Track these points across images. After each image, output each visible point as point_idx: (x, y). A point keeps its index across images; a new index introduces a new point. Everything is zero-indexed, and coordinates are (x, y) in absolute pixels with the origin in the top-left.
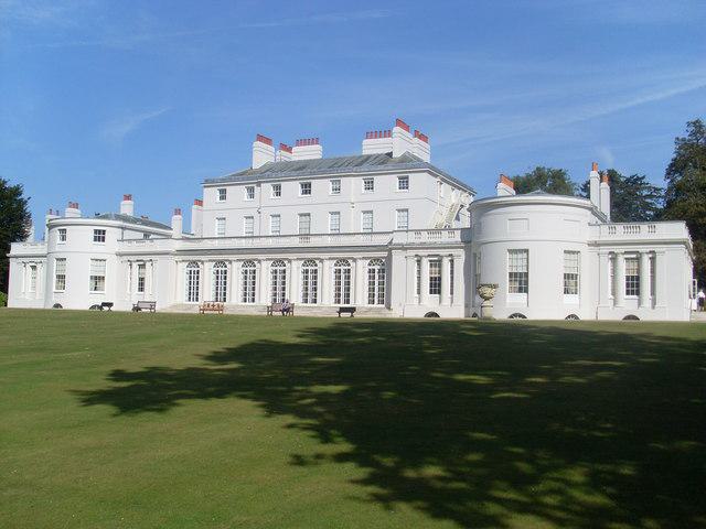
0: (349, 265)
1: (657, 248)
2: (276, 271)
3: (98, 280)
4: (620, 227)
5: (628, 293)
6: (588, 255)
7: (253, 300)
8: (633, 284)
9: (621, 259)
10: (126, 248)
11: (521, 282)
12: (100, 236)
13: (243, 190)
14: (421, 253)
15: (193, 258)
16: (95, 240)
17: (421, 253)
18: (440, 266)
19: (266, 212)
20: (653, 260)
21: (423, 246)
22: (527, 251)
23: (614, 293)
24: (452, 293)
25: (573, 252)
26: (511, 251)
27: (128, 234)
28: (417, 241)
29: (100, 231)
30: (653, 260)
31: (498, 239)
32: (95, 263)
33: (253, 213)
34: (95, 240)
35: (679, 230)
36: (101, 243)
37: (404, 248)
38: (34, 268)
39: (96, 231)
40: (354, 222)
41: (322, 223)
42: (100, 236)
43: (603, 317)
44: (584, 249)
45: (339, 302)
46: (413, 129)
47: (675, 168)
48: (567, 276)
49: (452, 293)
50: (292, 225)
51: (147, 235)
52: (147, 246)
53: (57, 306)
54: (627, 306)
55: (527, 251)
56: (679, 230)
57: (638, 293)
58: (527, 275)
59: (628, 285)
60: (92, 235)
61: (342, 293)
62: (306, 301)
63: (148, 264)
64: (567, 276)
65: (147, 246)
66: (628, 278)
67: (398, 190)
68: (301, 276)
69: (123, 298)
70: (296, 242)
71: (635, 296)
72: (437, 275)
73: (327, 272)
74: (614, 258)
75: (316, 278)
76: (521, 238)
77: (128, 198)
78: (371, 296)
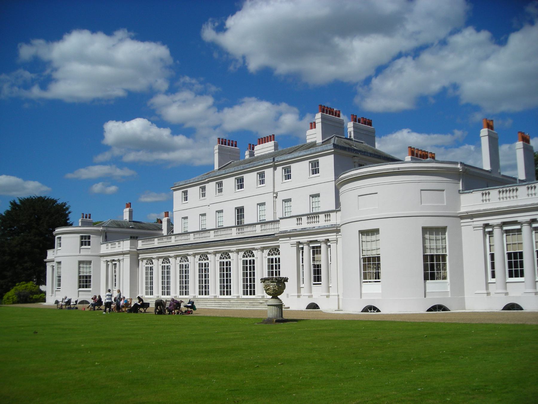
36: (87, 247)
39: (82, 237)
70: (234, 234)
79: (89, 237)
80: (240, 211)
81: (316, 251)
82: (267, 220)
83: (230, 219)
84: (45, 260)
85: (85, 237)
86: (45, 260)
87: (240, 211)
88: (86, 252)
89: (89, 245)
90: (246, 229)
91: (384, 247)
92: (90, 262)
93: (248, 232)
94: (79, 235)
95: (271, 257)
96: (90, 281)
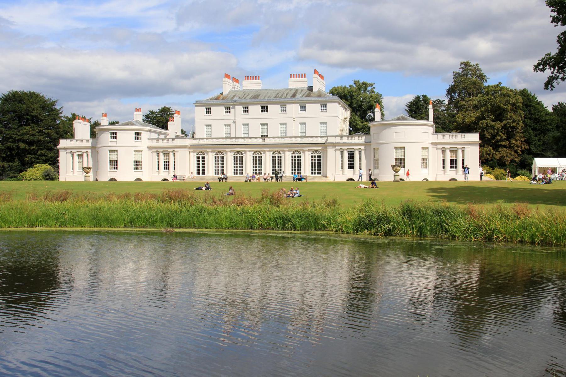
1: (175, 150)
3: (137, 164)
4: (440, 135)
5: (451, 167)
6: (432, 149)
7: (204, 174)
9: (75, 155)
10: (154, 143)
11: (115, 164)
12: (137, 136)
13: (278, 107)
14: (343, 148)
17: (343, 148)
18: (169, 156)
19: (239, 123)
20: (463, 151)
21: (345, 144)
22: (404, 148)
23: (342, 168)
24: (174, 169)
25: (139, 151)
26: (396, 148)
28: (341, 141)
29: (138, 133)
30: (463, 151)
32: (136, 153)
33: (231, 122)
35: (474, 137)
37: (334, 145)
39: (136, 134)
40: (294, 130)
41: (275, 131)
43: (439, 179)
44: (430, 146)
45: (218, 174)
46: (231, 78)
47: (451, 91)
48: (423, 159)
49: (174, 169)
50: (256, 131)
53: (112, 179)
54: (164, 174)
55: (404, 148)
56: (474, 137)
57: (456, 167)
58: (404, 159)
59: (349, 164)
62: (199, 174)
64: (423, 159)
66: (451, 160)
67: (300, 112)
68: (196, 162)
69: (151, 173)
71: (454, 169)
72: (403, 157)
73: (210, 159)
74: (444, 152)
75: (204, 161)
76: (397, 141)
78: (217, 171)
92: (374, 149)
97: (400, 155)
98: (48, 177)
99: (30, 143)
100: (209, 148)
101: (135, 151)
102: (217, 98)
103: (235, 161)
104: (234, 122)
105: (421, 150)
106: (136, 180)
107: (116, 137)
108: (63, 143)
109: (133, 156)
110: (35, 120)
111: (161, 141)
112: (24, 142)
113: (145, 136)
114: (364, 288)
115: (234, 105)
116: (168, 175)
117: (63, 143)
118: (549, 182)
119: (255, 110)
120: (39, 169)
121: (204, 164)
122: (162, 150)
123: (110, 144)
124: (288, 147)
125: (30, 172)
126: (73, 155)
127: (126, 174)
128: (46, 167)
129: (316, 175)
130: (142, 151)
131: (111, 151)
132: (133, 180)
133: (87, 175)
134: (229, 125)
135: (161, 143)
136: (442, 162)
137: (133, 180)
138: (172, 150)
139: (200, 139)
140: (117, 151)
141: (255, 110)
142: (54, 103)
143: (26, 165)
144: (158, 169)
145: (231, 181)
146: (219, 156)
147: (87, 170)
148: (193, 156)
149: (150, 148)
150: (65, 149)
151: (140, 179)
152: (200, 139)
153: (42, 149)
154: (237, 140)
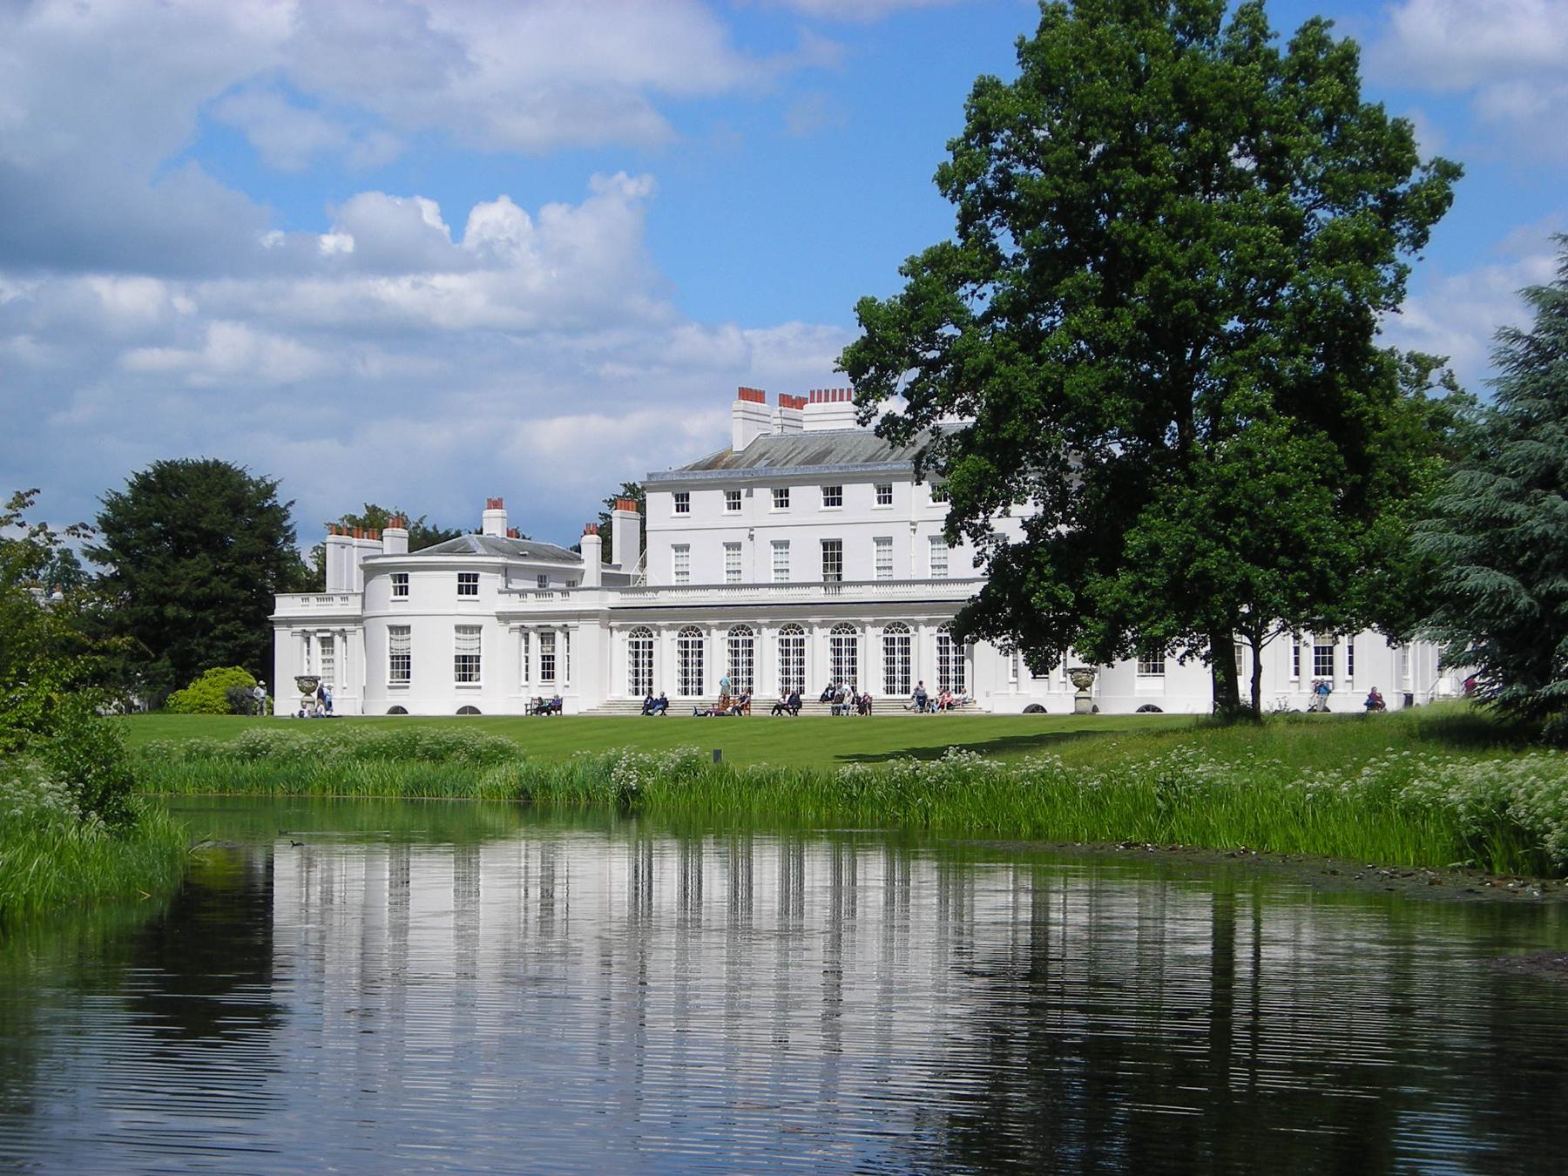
0: (907, 631)
2: (737, 642)
3: (467, 668)
7: (700, 692)
8: (832, 566)
9: (533, 637)
10: (514, 604)
12: (468, 584)
15: (640, 626)
16: (460, 592)
19: (765, 537)
27: (517, 584)
31: (1201, 987)
33: (741, 536)
34: (460, 592)
36: (471, 597)
38: (327, 643)
39: (461, 577)
42: (468, 584)
51: (542, 580)
52: (556, 603)
53: (398, 710)
60: (456, 582)
61: (898, 676)
63: (338, 639)
65: (556, 603)
69: (504, 692)
70: (818, 595)
77: (496, 504)
78: (890, 680)
79: (476, 577)
80: (832, 551)
81: (547, 637)
82: (895, 578)
83: (810, 565)
84: (270, 617)
85: (468, 577)
86: (270, 617)
87: (832, 551)
88: (468, 609)
89: (475, 593)
90: (845, 590)
91: (416, 646)
92: (479, 628)
93: (848, 594)
94: (456, 574)
95: (837, 636)
96: (457, 669)
97: (468, 648)
98: (240, 705)
99: (200, 605)
100: (919, 612)
101: (458, 628)
102: (710, 465)
103: (889, 651)
104: (751, 537)
105: (454, 633)
106: (463, 710)
107: (475, 587)
108: (287, 605)
109: (454, 643)
110: (212, 542)
111: (531, 596)
112: (184, 601)
113: (489, 583)
114: (1045, 1006)
115: (750, 487)
116: (468, 698)
117: (287, 605)
118: (950, 706)
119: (806, 498)
120: (215, 683)
121: (907, 661)
122: (534, 624)
123: (393, 609)
124: (925, 612)
125: (195, 690)
126: (308, 640)
127: (433, 696)
128: (239, 676)
129: (898, 696)
130: (479, 628)
131: (393, 629)
132: (451, 711)
133: (1083, 694)
134: (738, 546)
135: (533, 604)
136: (1292, 656)
137: (452, 712)
138: (560, 624)
139: (656, 589)
140: (408, 628)
141: (806, 498)
142: (269, 491)
143: (186, 673)
144: (1297, 672)
145: (574, 712)
146: (896, 636)
147: (1084, 677)
148: (620, 643)
149: (504, 617)
150: (289, 622)
151: (473, 710)
152: (656, 589)
153: (227, 621)
154: (691, 593)
